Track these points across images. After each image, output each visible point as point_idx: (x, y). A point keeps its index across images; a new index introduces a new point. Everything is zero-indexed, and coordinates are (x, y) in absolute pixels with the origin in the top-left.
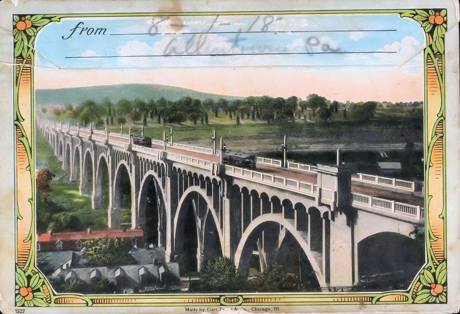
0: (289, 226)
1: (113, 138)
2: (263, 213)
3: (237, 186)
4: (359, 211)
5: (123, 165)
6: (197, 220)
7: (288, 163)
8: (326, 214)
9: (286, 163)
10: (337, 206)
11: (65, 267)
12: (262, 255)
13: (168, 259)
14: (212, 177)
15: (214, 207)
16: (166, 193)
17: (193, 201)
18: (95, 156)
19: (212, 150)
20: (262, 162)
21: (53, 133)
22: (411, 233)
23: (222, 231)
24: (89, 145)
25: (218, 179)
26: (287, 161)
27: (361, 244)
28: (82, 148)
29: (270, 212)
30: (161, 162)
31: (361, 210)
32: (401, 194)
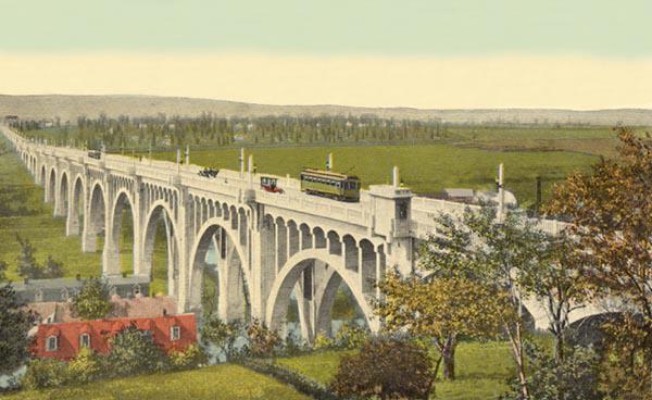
0: (338, 263)
8: (381, 247)
24: (79, 169)
25: (246, 208)
29: (310, 247)
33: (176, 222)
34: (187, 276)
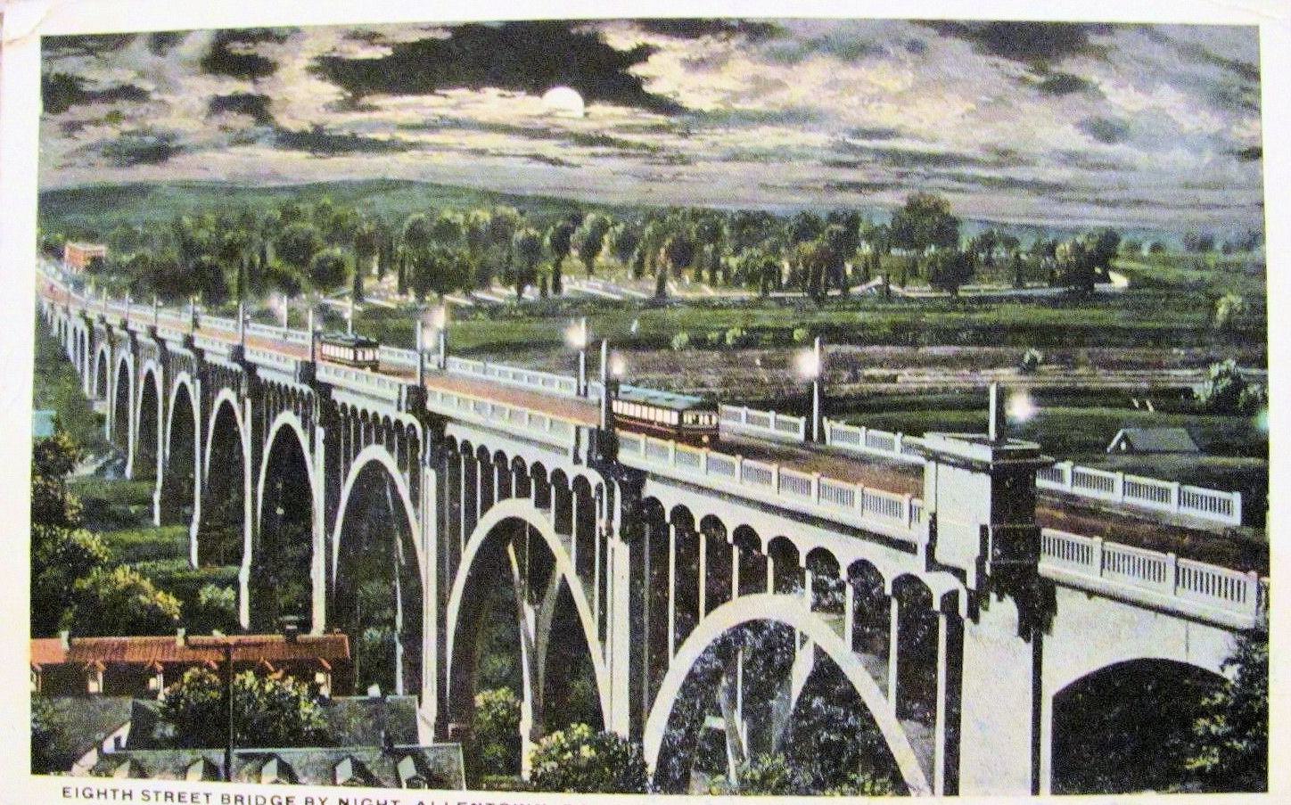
1: (260, 342)
2: (740, 595)
3: (654, 502)
4: (1060, 591)
5: (287, 430)
6: (524, 617)
7: (827, 424)
8: (951, 599)
9: (821, 429)
10: (988, 571)
11: (109, 746)
12: (735, 733)
13: (426, 737)
14: (572, 472)
15: (579, 571)
16: (420, 521)
17: (511, 550)
18: (254, 431)
19: (574, 380)
20: (743, 426)
21: (82, 327)
22: (1231, 661)
23: (604, 647)
25: (594, 478)
26: (825, 419)
27: (1064, 701)
28: (166, 372)
29: (761, 588)
30: (408, 419)
31: (1063, 585)
32: (1195, 534)
33: (676, 652)
34: (164, 453)
